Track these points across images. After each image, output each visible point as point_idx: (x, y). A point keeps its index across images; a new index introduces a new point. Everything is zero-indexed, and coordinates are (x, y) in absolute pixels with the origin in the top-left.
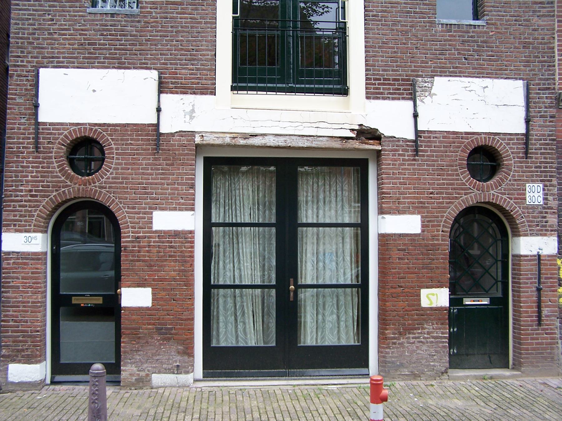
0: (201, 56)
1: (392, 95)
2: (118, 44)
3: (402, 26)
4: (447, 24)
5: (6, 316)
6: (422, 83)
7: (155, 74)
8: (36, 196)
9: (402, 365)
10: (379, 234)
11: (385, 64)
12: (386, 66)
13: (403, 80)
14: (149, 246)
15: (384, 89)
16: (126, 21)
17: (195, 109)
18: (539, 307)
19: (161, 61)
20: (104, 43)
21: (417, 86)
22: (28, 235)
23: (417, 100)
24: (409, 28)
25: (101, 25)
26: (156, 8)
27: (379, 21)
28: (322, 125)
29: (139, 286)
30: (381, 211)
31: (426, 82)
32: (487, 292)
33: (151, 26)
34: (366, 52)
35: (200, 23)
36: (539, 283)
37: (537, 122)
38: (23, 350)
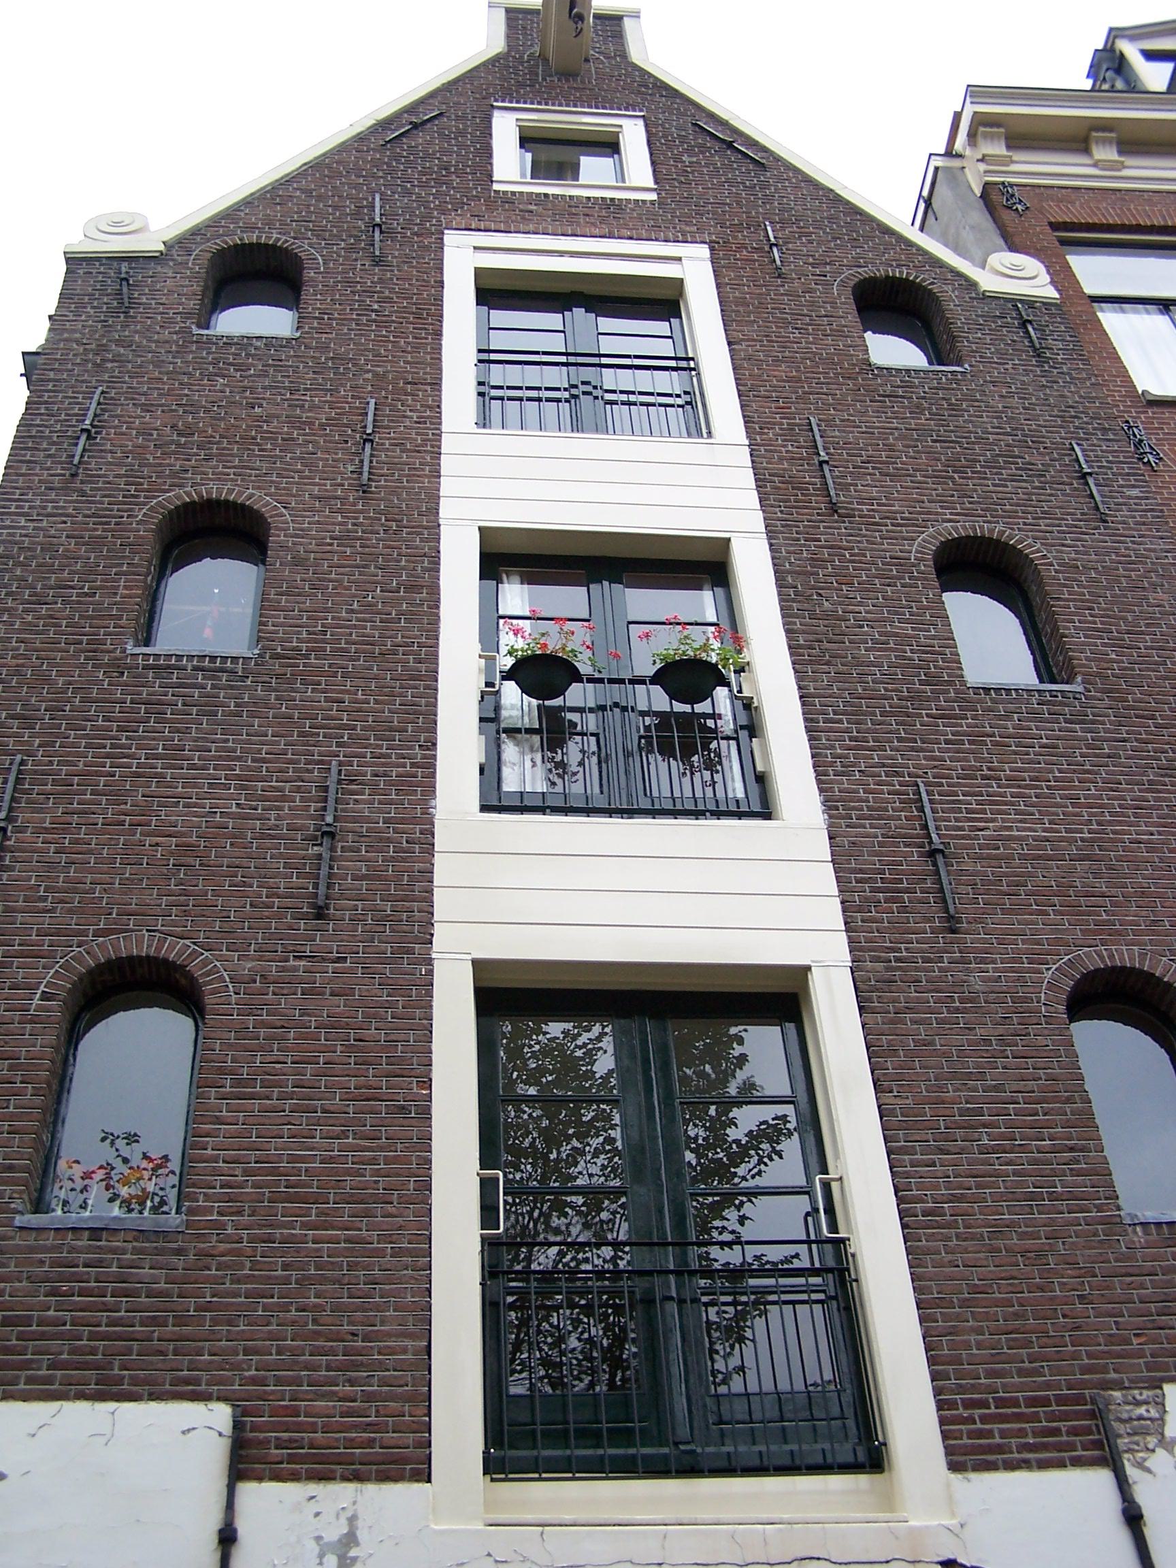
0: (380, 1353)
1: (1036, 1452)
2: (104, 1321)
3: (1023, 1236)
4: (1158, 1224)
6: (1128, 1408)
7: (220, 1415)
11: (992, 1355)
12: (994, 1359)
13: (1061, 1400)
15: (1003, 1435)
16: (136, 1251)
17: (358, 1533)
19: (247, 1374)
20: (57, 1318)
21: (1111, 1417)
23: (1126, 1462)
24: (1044, 1241)
25: (55, 1263)
26: (239, 1213)
27: (949, 1226)
31: (1138, 1403)
33: (219, 1264)
34: (922, 1320)
35: (380, 1253)
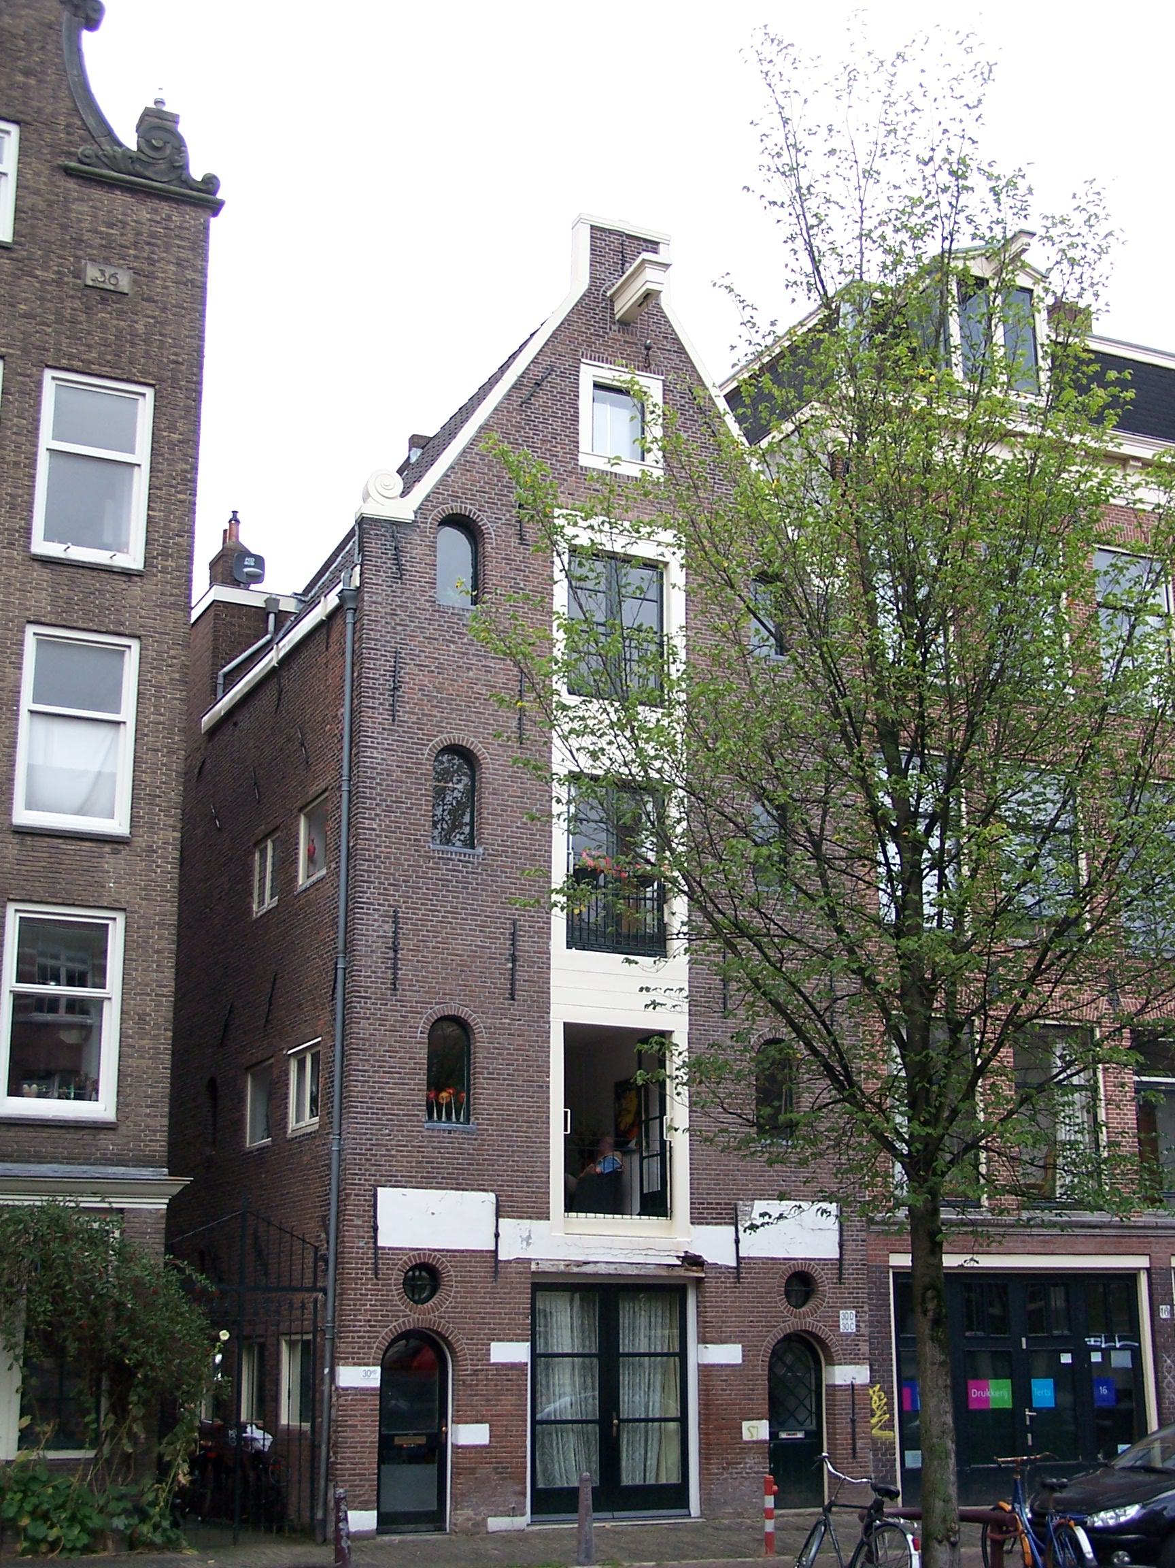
5: (343, 1458)
7: (491, 1197)
8: (374, 1326)
9: (725, 1502)
10: (699, 1365)
14: (487, 1380)
18: (854, 1439)
22: (366, 1368)
28: (650, 1252)
29: (477, 1422)
30: (703, 1340)
32: (802, 1424)
36: (854, 1414)
37: (850, 1246)
38: (360, 1496)
